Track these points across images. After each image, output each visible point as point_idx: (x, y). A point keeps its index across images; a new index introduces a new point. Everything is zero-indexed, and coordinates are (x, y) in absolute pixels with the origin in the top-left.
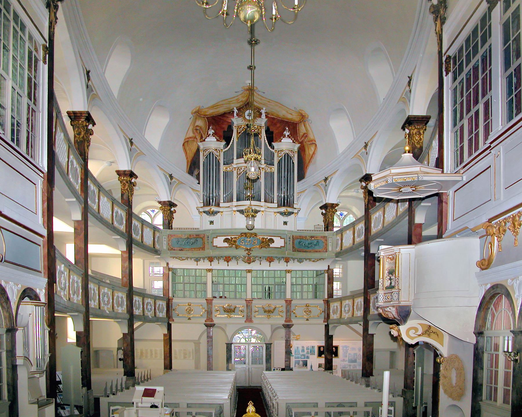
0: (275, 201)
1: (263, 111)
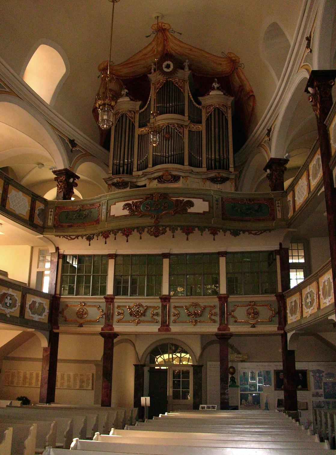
0: (204, 165)
1: (186, 64)
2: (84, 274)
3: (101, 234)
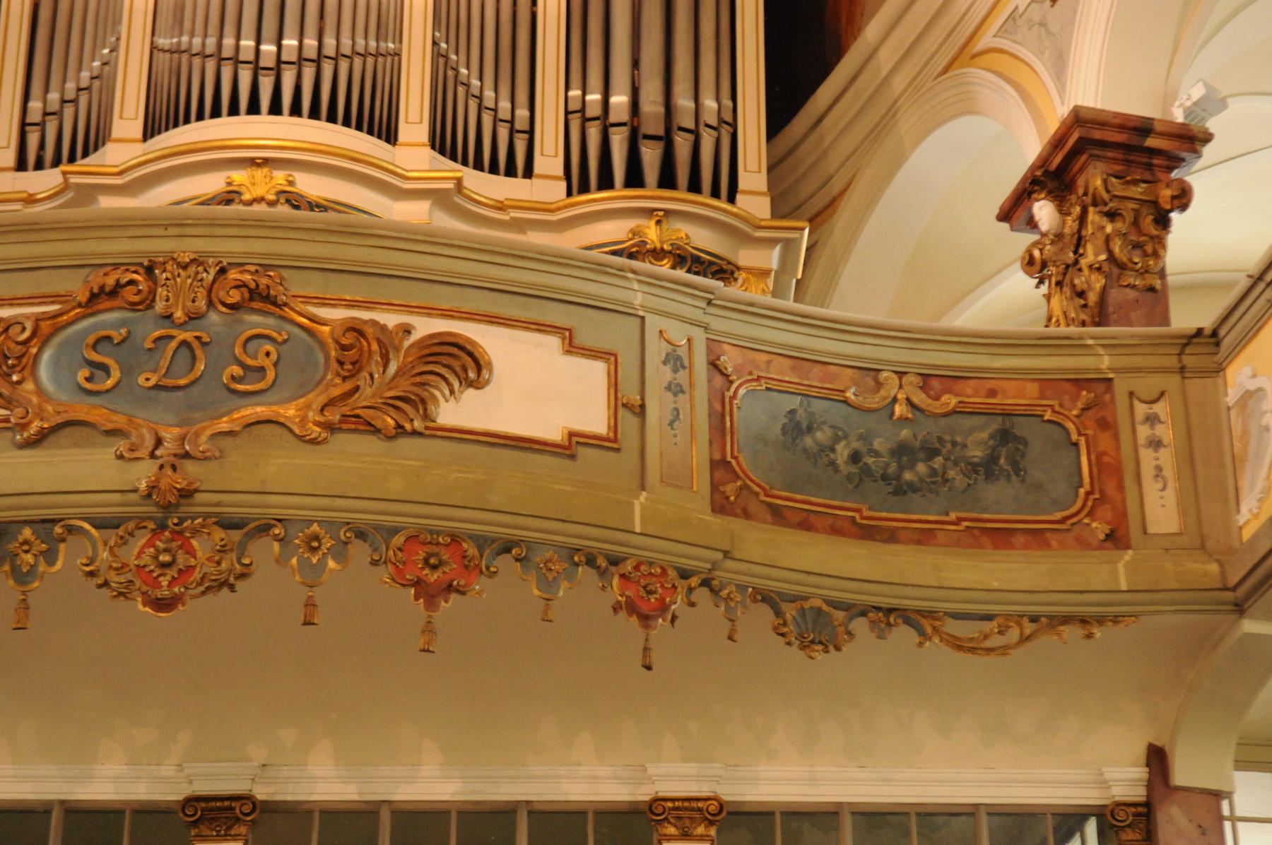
0: (549, 160)
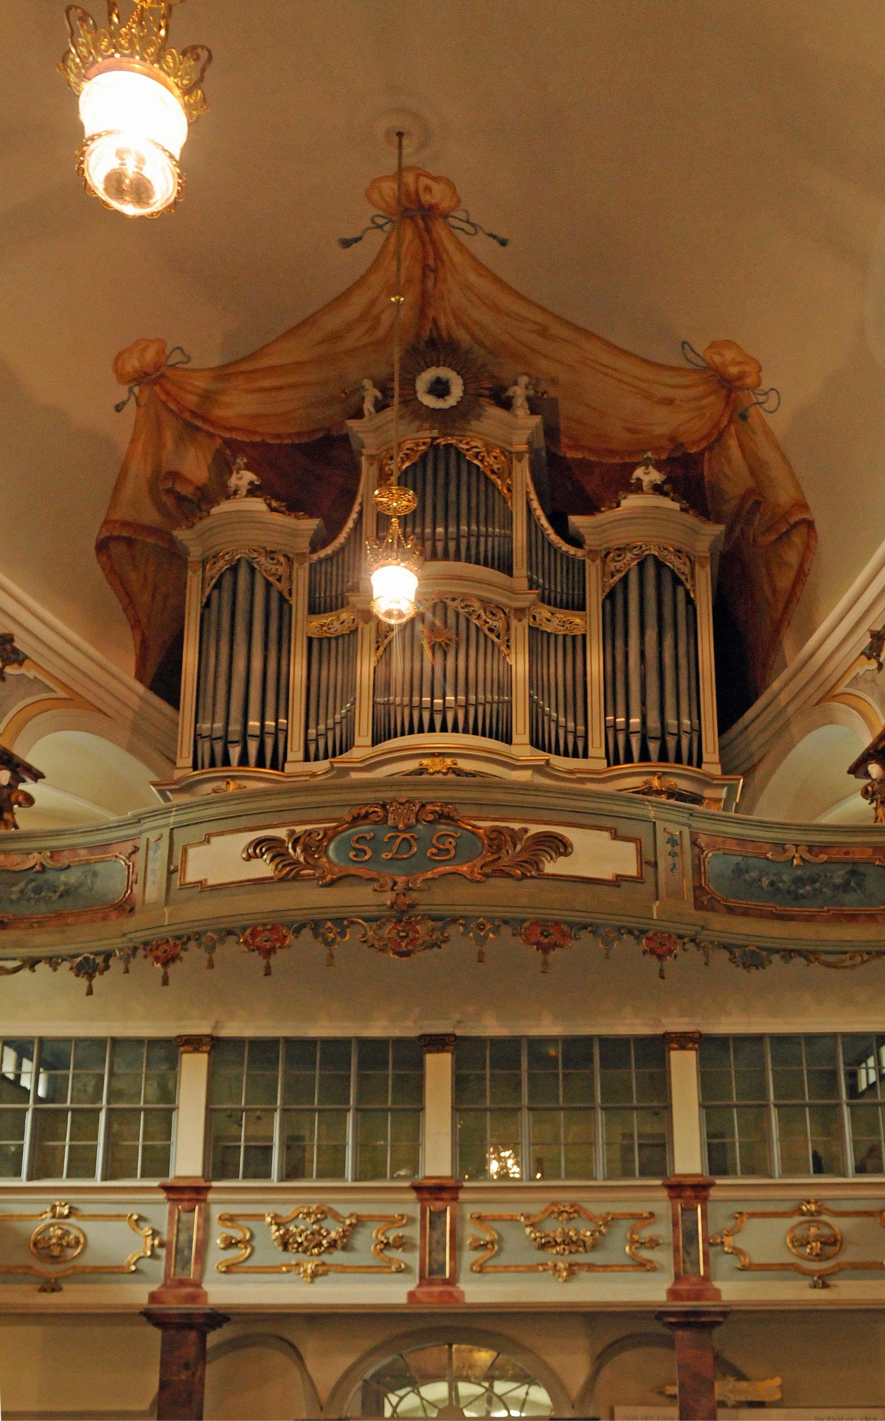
0: (597, 748)
2: (68, 1104)
3: (141, 953)
